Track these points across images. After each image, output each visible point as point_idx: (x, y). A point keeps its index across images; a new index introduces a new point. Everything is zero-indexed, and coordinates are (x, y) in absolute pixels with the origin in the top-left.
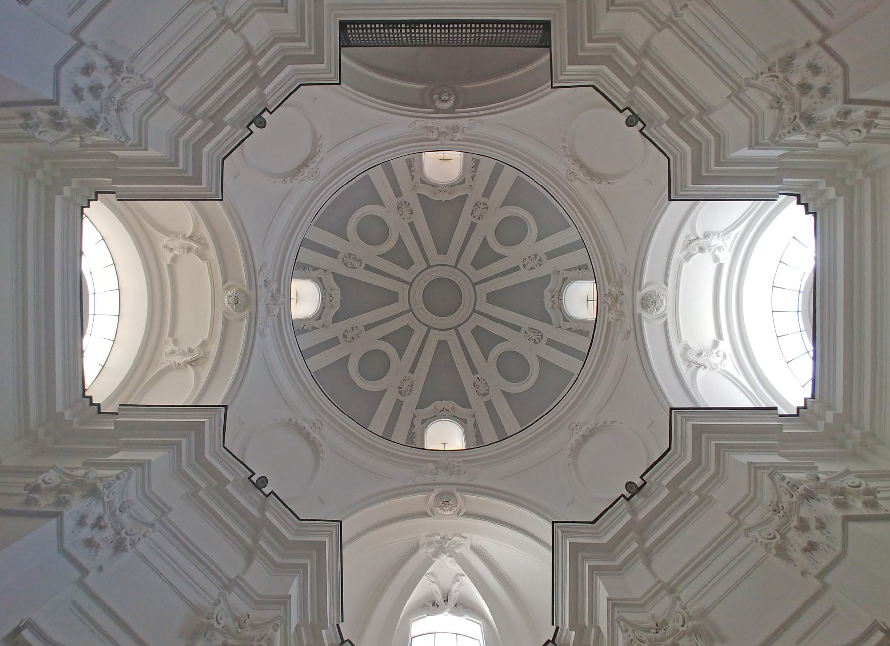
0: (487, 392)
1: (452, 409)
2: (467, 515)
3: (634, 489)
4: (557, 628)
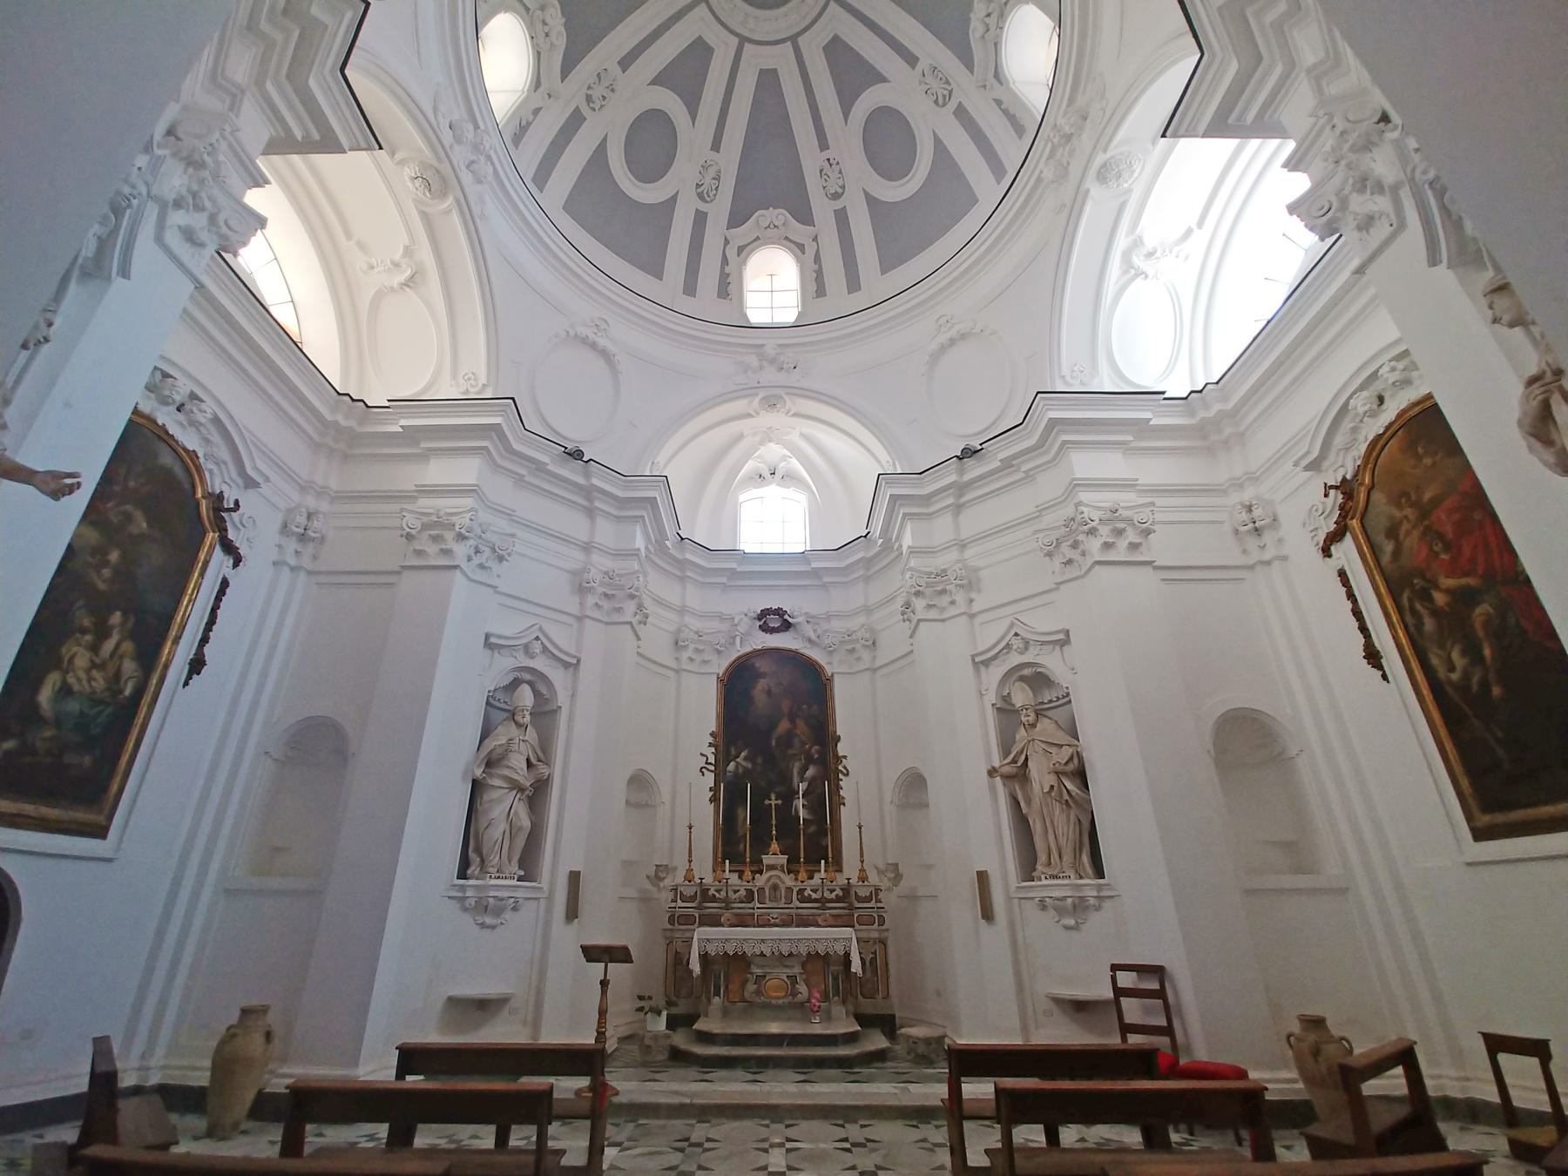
0: (840, 191)
1: (784, 224)
2: (796, 415)
3: (968, 453)
4: (869, 533)
